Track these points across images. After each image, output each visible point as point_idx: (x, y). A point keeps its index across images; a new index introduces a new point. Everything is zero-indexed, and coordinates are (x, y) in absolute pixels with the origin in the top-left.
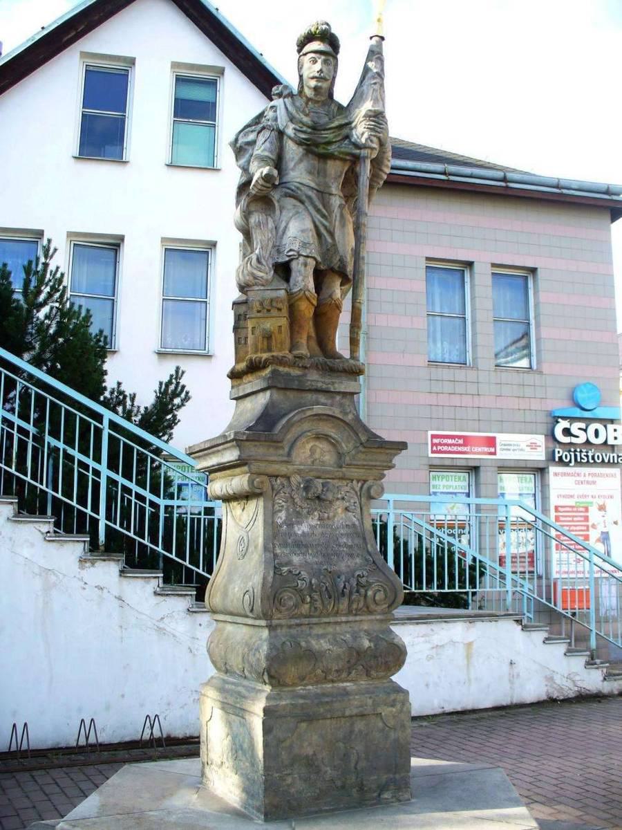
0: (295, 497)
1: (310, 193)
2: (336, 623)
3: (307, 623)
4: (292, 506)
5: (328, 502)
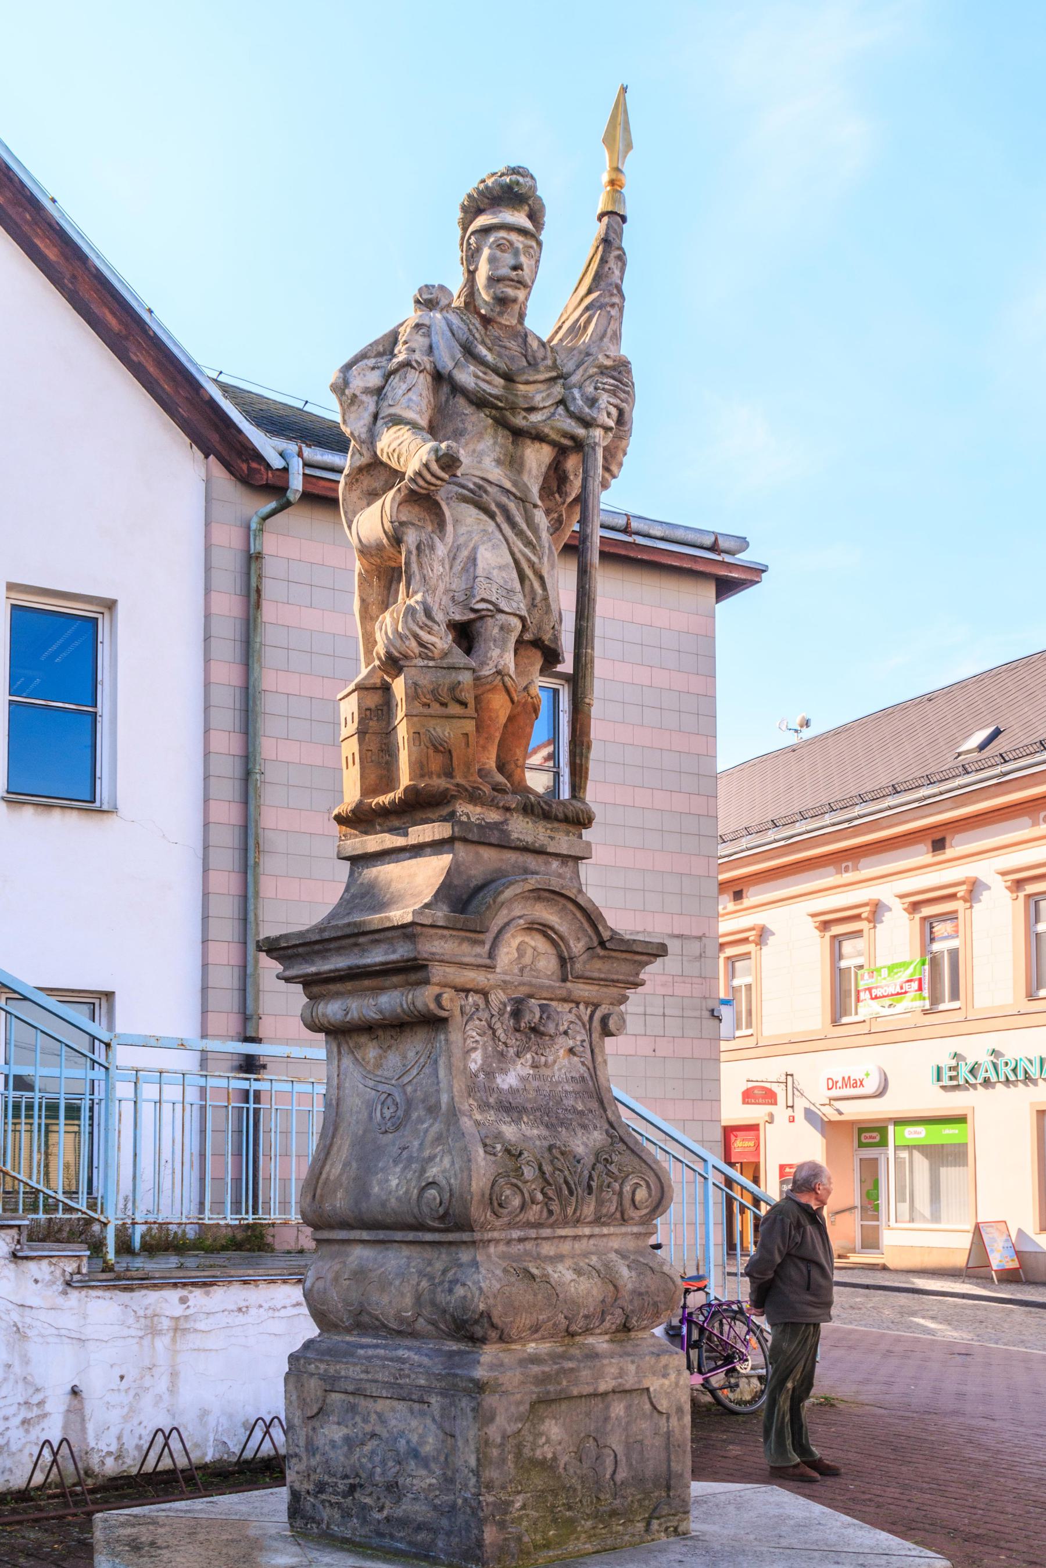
0: (496, 1027)
1: (504, 500)
2: (576, 1238)
3: (534, 1236)
4: (491, 1043)
5: (547, 1038)
